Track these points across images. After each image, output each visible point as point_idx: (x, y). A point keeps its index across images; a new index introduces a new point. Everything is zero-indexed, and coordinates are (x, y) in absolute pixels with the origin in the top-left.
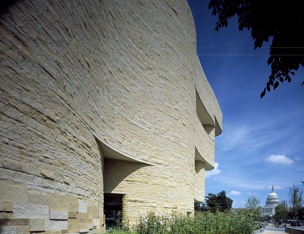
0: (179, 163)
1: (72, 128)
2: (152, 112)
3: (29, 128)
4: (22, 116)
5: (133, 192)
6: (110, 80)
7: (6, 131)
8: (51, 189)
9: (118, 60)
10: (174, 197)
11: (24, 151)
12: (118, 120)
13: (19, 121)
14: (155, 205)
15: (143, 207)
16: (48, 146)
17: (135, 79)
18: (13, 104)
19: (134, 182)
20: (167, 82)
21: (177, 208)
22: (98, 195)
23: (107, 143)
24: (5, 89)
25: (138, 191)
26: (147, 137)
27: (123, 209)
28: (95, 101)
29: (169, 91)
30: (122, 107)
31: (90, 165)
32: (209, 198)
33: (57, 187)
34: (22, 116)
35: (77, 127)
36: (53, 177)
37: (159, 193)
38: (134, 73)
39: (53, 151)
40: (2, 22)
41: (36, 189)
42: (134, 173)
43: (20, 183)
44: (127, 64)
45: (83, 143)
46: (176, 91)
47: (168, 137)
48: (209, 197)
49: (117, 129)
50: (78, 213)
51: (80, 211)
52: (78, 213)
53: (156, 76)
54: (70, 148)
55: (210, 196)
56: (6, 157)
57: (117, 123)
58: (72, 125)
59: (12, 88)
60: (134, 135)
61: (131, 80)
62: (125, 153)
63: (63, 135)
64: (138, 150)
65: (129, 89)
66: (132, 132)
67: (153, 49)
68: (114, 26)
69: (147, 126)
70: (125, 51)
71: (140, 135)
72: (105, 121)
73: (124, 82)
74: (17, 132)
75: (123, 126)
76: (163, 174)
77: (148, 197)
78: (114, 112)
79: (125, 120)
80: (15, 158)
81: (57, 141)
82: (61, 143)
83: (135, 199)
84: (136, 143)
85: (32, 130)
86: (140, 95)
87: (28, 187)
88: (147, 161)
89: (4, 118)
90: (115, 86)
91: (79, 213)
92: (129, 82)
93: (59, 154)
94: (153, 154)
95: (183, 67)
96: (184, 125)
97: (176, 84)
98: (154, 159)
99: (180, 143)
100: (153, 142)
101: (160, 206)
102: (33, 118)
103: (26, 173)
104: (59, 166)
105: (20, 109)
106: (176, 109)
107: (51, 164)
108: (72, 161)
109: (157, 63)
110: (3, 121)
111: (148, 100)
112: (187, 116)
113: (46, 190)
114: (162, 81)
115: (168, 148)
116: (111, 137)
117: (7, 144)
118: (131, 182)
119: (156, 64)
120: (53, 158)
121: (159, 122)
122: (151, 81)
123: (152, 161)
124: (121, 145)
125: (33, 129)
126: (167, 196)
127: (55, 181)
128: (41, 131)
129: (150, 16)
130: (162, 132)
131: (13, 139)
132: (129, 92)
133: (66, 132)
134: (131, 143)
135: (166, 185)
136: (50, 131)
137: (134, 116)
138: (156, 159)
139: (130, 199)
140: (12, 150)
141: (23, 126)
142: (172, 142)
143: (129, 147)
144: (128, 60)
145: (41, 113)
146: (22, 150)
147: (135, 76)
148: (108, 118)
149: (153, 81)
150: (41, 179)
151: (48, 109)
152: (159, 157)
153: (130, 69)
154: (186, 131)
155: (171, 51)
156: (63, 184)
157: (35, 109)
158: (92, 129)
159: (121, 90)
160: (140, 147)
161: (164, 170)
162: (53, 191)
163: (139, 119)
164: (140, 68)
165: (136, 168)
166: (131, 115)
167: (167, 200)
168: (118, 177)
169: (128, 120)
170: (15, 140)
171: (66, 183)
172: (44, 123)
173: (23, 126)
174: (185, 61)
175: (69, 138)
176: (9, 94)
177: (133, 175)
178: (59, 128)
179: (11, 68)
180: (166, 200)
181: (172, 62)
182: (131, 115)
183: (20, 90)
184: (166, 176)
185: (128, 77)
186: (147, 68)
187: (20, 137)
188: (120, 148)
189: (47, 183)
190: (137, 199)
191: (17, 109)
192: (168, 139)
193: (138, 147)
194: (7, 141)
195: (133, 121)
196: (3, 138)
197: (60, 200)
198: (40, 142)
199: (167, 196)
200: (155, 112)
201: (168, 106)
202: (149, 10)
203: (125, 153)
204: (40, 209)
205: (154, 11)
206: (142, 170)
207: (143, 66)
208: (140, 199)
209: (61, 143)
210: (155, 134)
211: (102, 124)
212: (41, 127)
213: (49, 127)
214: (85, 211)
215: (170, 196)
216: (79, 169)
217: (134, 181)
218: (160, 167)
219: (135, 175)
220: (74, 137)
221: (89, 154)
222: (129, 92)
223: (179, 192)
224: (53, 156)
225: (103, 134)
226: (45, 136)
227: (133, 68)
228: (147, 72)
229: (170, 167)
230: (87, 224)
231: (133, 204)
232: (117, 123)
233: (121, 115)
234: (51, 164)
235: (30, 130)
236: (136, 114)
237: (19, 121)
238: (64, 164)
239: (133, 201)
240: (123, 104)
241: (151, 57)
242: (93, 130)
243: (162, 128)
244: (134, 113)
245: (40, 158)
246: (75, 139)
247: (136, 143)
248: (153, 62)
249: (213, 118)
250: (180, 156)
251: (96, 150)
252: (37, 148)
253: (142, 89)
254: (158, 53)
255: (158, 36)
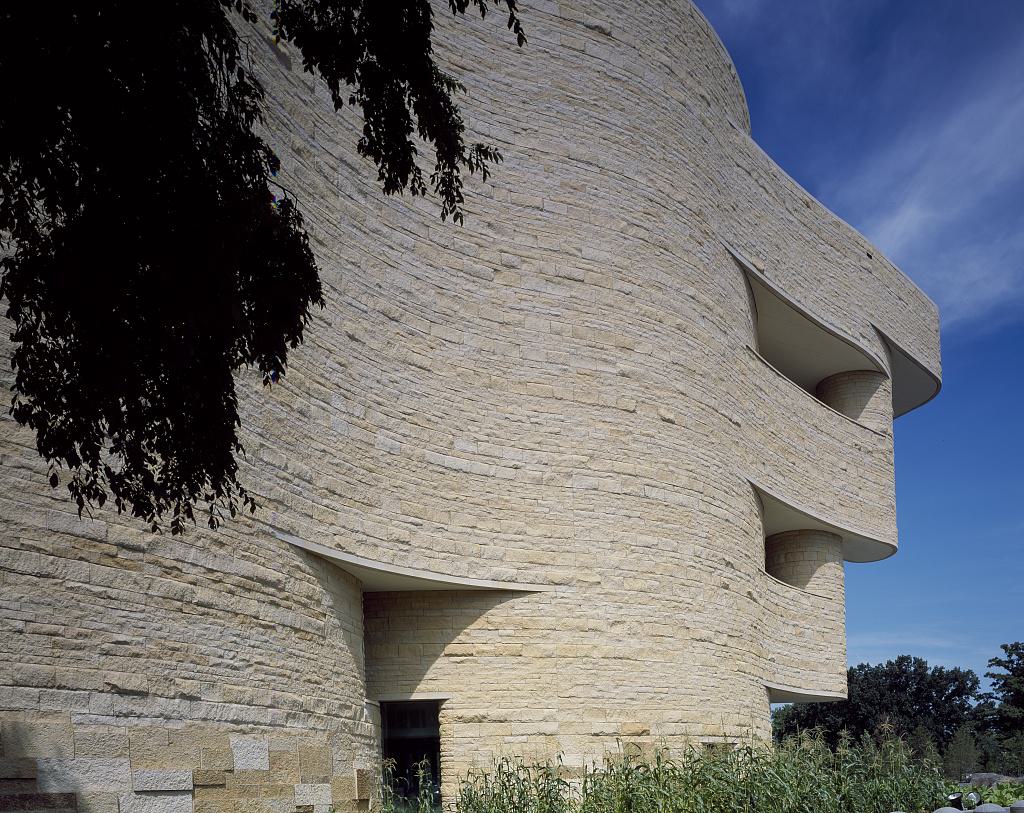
0: (647, 565)
1: (203, 549)
2: (522, 412)
3: (71, 584)
4: (52, 563)
5: (471, 689)
6: (352, 359)
7: (17, 605)
8: (139, 717)
9: (380, 287)
10: (632, 695)
11: (61, 638)
12: (390, 471)
13: (48, 576)
14: (551, 727)
15: (507, 739)
16: (124, 613)
17: (450, 319)
18: (30, 543)
19: (470, 658)
20: (577, 290)
21: (645, 732)
22: (328, 714)
23: (350, 553)
24: (12, 516)
25: (486, 687)
26: (506, 501)
27: (442, 747)
28: (290, 447)
29: (586, 317)
30: (405, 428)
31: (281, 632)
32: (1007, 667)
33: (157, 710)
34: (52, 563)
35: (221, 543)
36: (144, 686)
37: (564, 685)
38: (443, 303)
39: (141, 624)
40: (5, 379)
41: (96, 722)
42: (471, 627)
43: (56, 712)
44: (414, 286)
45: (247, 578)
46: (621, 309)
47: (593, 481)
48: (1012, 662)
49: (386, 499)
50: (231, 771)
51: (239, 766)
52: (231, 771)
53: (532, 283)
54: (197, 604)
55: (1014, 657)
56: (20, 661)
57: (386, 484)
58: (200, 543)
59: (28, 509)
60: (454, 506)
61: (436, 330)
62: (424, 570)
63: (169, 576)
64: (475, 549)
65: (426, 363)
66: (448, 497)
67: (514, 196)
68: (360, 192)
69: (505, 463)
70: (407, 248)
71: (479, 501)
72: (338, 492)
73: (410, 345)
74: (42, 600)
75: (412, 487)
76: (579, 617)
77: (524, 702)
78: (373, 452)
79: (419, 464)
80: (40, 658)
81: (152, 597)
82: (164, 598)
83: (476, 714)
84: (465, 529)
85: (79, 587)
86: (472, 367)
87: (74, 719)
88: (513, 581)
89: (12, 578)
90: (373, 372)
91: (236, 772)
92: (428, 337)
93: (158, 625)
94: (534, 553)
95: (651, 210)
96: (669, 421)
97: (619, 285)
98: (541, 571)
99: (653, 493)
100: (533, 511)
101: (571, 730)
102: (81, 559)
103: (69, 689)
104: (159, 658)
105: (48, 549)
106: (623, 375)
107: (137, 655)
108: (206, 637)
109: (532, 240)
110: (10, 585)
111: (505, 373)
112: (680, 387)
113: (123, 721)
114: (559, 293)
115: (595, 523)
116: (364, 533)
117: (21, 632)
118: (463, 658)
119: (530, 241)
120: (141, 639)
121: (553, 440)
122: (515, 306)
123: (531, 578)
124: (406, 547)
125: (80, 584)
126: (600, 694)
127: (150, 696)
128: (102, 584)
129: (499, 94)
130: (566, 470)
131: (32, 619)
132: (429, 370)
133: (179, 565)
134: (447, 534)
135: (595, 653)
136: (129, 576)
137: (452, 443)
138: (549, 568)
139: (460, 713)
140: (32, 644)
141: (56, 584)
142: (613, 496)
143: (438, 548)
144: (421, 270)
145: (101, 541)
146: (54, 638)
147: (449, 312)
148: (348, 479)
149: (524, 305)
150: (106, 698)
151: (121, 524)
152: (559, 561)
153: (430, 296)
154: (678, 441)
155: (593, 174)
156: (177, 701)
157: (83, 537)
158: (281, 530)
159: (396, 376)
160: (482, 541)
161: (580, 602)
162: (146, 723)
163: (472, 448)
164: (468, 277)
165: (477, 611)
166: (441, 444)
167: (600, 706)
168: (421, 647)
169: (432, 461)
170: (39, 620)
171: (184, 696)
172: (109, 561)
173: (56, 584)
174: (660, 183)
175: (191, 578)
176: (21, 524)
177: (468, 635)
178: (155, 563)
179: (24, 467)
180: (594, 706)
181: (595, 211)
182: (441, 444)
183: (46, 505)
184: (592, 624)
185: (418, 326)
186: (495, 270)
187: (51, 611)
188: (402, 558)
189: (124, 704)
190: (482, 712)
191: (39, 550)
192: (595, 489)
193: (473, 539)
194: (20, 625)
195: (449, 461)
196: (11, 622)
197: (167, 743)
198: (102, 609)
199: (600, 694)
200: (535, 408)
201: (588, 372)
202: (493, 74)
203: (424, 570)
204: (105, 769)
205: (511, 69)
206: (498, 613)
207: (478, 267)
208: (494, 713)
209: (164, 598)
210: (539, 482)
211: (326, 502)
212: (103, 572)
213: (126, 568)
214: (261, 764)
215: (617, 691)
216: (232, 654)
217: (472, 655)
218: (563, 595)
219: (479, 635)
220: (211, 571)
221: (272, 603)
222: (429, 370)
223: (656, 675)
224: (140, 635)
225: (332, 530)
226: (113, 593)
227: (440, 290)
228: (498, 280)
229: (607, 587)
230: (269, 800)
231: (472, 730)
232: (386, 484)
233: (402, 452)
234: (137, 655)
235: (72, 588)
236: (459, 433)
237: (48, 576)
238: (175, 649)
239: (471, 721)
240: (407, 417)
241: (509, 225)
242: (288, 533)
243: (566, 457)
244: (454, 431)
245: (103, 646)
246: (213, 576)
247: (465, 529)
248: (518, 240)
249: (863, 344)
250: (650, 540)
251: (307, 585)
252: (95, 625)
253: (480, 345)
254: (537, 202)
255: (533, 143)
